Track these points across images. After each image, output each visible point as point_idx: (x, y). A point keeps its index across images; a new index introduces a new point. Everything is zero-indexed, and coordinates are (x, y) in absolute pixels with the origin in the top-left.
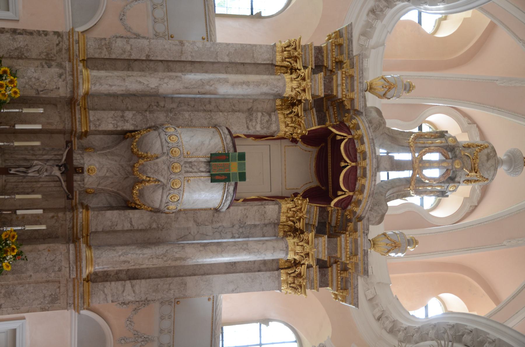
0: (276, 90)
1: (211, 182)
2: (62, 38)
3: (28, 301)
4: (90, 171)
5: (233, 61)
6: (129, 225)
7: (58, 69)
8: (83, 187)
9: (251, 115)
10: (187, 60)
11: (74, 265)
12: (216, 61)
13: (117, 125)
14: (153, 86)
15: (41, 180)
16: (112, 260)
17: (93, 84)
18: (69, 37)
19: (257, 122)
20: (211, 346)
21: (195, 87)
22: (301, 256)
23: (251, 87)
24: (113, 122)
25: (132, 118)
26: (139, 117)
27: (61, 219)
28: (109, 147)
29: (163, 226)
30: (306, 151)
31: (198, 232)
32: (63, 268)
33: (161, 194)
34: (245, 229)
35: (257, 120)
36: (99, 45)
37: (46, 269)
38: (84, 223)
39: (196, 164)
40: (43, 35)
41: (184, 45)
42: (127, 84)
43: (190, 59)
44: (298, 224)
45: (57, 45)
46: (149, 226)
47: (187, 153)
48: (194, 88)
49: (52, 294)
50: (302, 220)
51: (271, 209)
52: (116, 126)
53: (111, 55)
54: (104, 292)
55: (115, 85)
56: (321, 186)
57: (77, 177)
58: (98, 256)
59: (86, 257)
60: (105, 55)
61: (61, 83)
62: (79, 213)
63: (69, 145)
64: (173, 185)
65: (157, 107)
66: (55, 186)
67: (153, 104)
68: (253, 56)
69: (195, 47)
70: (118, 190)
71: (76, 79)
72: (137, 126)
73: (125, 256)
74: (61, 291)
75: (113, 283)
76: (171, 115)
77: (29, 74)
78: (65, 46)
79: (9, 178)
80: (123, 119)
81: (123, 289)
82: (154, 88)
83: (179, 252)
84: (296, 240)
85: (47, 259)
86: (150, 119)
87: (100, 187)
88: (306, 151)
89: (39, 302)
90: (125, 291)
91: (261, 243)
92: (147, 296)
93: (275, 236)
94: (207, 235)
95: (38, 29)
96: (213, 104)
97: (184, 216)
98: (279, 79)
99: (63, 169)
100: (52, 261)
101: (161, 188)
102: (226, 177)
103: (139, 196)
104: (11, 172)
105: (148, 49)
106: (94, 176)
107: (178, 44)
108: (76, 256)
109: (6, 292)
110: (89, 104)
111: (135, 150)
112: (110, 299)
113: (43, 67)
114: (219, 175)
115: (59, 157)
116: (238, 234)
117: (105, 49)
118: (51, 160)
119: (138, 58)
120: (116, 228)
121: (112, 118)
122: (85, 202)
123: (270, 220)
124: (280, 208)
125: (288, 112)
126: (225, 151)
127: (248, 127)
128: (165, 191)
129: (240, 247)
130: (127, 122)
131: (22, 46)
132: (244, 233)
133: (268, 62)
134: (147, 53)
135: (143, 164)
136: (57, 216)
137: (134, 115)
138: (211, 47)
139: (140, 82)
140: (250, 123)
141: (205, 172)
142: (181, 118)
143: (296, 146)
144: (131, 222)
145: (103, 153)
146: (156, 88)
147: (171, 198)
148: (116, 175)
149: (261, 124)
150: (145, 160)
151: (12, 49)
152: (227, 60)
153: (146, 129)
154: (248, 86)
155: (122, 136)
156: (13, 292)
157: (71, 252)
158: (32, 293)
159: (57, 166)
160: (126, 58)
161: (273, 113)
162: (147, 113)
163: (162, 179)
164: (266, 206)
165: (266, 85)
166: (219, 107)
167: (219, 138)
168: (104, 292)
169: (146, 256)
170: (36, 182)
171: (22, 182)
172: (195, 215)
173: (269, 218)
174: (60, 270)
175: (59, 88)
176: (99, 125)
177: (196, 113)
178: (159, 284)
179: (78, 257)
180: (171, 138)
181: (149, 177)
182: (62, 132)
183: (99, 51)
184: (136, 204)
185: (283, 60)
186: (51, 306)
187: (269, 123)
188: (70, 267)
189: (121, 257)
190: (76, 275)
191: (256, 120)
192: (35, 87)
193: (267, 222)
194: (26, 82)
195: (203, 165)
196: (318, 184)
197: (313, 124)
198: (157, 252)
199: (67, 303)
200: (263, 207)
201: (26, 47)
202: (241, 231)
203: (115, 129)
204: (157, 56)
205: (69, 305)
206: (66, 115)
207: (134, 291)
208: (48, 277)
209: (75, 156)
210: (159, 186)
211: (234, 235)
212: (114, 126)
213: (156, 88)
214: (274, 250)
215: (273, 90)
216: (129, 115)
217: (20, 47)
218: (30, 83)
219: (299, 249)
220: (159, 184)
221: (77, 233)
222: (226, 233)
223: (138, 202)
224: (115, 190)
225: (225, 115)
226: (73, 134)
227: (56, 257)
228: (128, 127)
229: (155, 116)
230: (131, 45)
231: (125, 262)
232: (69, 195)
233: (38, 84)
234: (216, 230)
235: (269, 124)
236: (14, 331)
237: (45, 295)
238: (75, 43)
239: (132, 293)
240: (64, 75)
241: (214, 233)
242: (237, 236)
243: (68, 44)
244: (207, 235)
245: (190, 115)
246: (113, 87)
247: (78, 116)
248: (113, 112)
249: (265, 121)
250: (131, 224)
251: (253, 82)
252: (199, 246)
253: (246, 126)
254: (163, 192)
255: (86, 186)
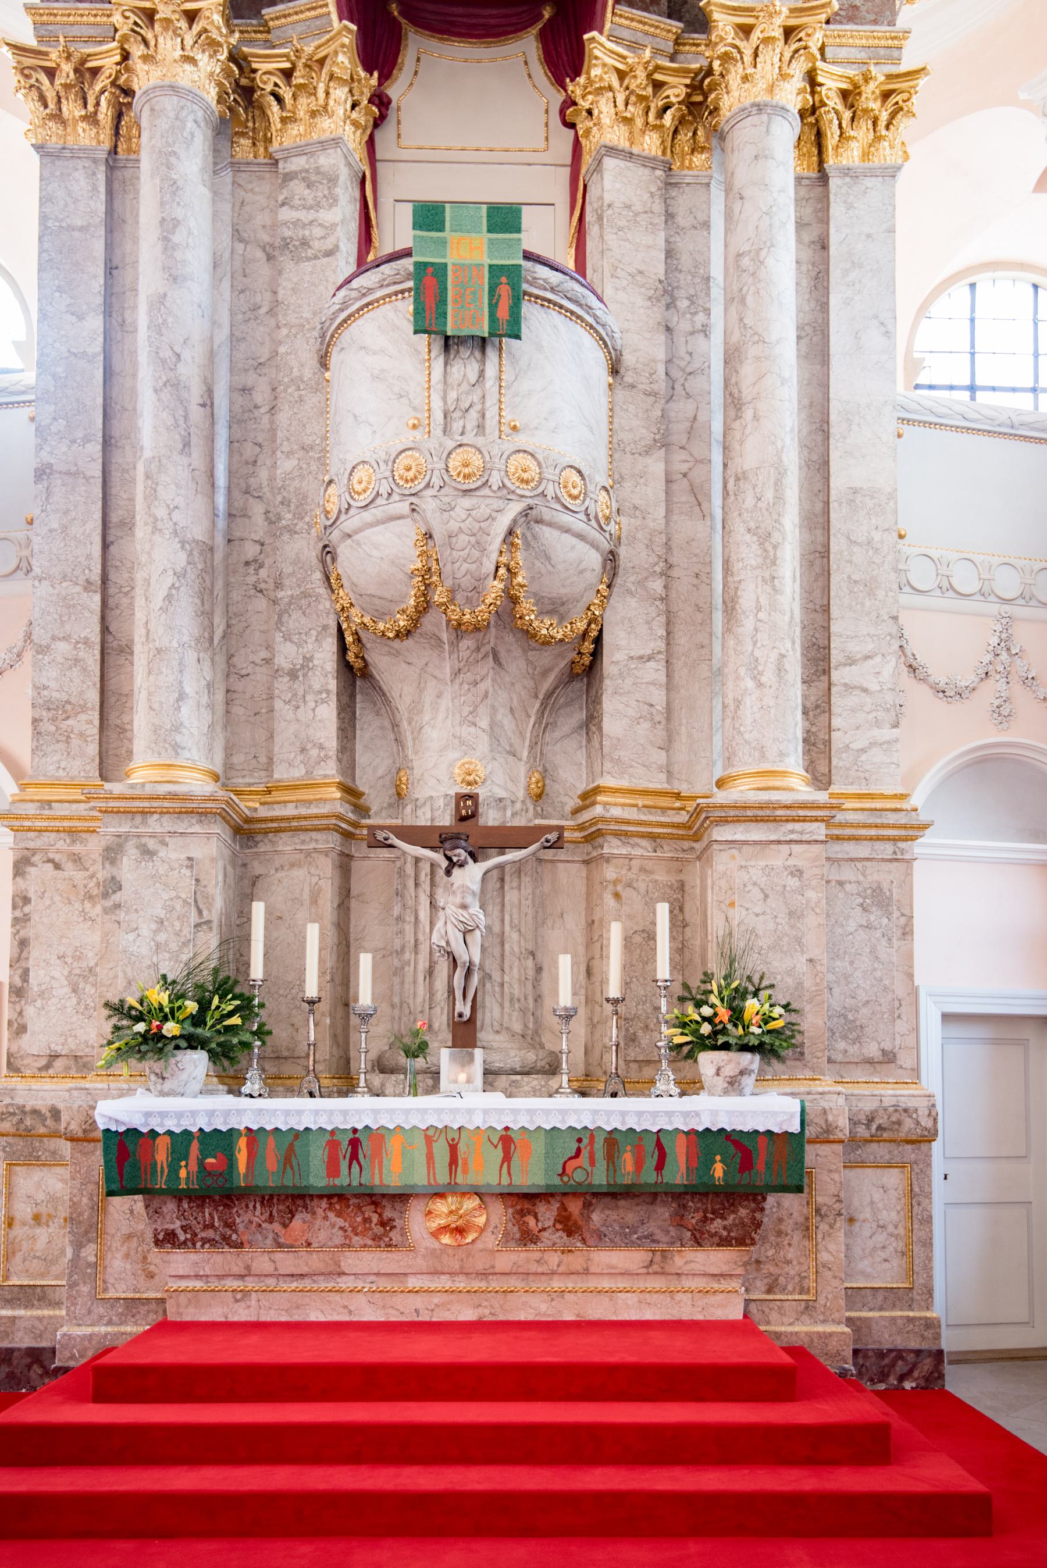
0: (190, 125)
1: (518, 337)
2: (34, 851)
3: (878, 974)
4: (471, 778)
5: (100, 300)
6: (652, 664)
7: (125, 859)
8: (523, 802)
9: (286, 244)
10: (99, 455)
11: (783, 829)
12: (102, 358)
13: (320, 692)
14: (183, 557)
15: (496, 929)
16: (773, 711)
17: (177, 754)
18: (30, 830)
19: (311, 223)
20: (1040, 441)
21: (181, 412)
22: (792, 57)
23: (179, 213)
24: (312, 704)
25: (299, 645)
26: (295, 621)
27: (624, 872)
28: (395, 725)
29: (659, 557)
30: (416, 73)
31: (682, 448)
32: (791, 862)
33: (556, 533)
34: (678, 287)
35: (306, 221)
36: (58, 742)
37: (791, 914)
38: (640, 803)
39: (452, 395)
40: (27, 909)
41: (50, 466)
42: (176, 645)
43: (95, 448)
44: (669, 92)
45: (57, 866)
46: (658, 603)
47: (414, 427)
48: (186, 418)
49: (861, 905)
50: (658, 76)
51: (618, 185)
52: (324, 695)
53: (89, 705)
54: (863, 751)
55: (181, 682)
56: (540, 25)
57: (490, 817)
58: (757, 754)
59: (758, 789)
60: (90, 722)
61: (174, 853)
62: (608, 815)
63: (380, 835)
64: (527, 482)
65: (261, 566)
66: (519, 888)
67: (252, 579)
68: (81, 229)
69: (54, 429)
70: (536, 696)
71: (155, 804)
72: (325, 627)
73: (760, 668)
74: (853, 878)
75: (836, 722)
76: (289, 516)
77: (144, 951)
78: (62, 843)
79: (487, 1021)
80: (300, 674)
81: (856, 692)
82: (190, 554)
83: (758, 490)
84: (734, 78)
85: (758, 910)
86: (299, 586)
87: (525, 754)
88: (416, 73)
89: (884, 942)
90: (865, 685)
91: (737, 206)
92: (886, 617)
93: (708, 185)
94: (695, 418)
95: (9, 922)
96: (250, 379)
97: (628, 484)
98: (152, 110)
99: (461, 854)
100: (766, 896)
101: (537, 528)
102: (504, 280)
103: (562, 619)
104: (467, 1013)
105: (65, 584)
106: (490, 767)
107: (45, 483)
108: (756, 820)
109: (844, 1037)
110: (252, 781)
111: (402, 623)
112: (886, 733)
113: (118, 906)
114: (493, 307)
115: (425, 868)
116: (696, 313)
117: (70, 722)
118: (432, 896)
119: (96, 619)
120: (660, 705)
121: (298, 707)
122: (573, 802)
123: (652, 195)
124: (612, 151)
125: (275, 107)
126: (409, 290)
127: (329, 254)
128: (547, 515)
129: (750, 280)
130: (310, 659)
131: (66, 973)
132: (692, 292)
133: (101, 177)
134: (78, 589)
135: (452, 591)
136: (615, 883)
137: (287, 638)
138: (54, 376)
139: (169, 598)
140: (316, 244)
141: (483, 361)
142: (296, 483)
143: (399, 109)
144: (641, 658)
145: (414, 739)
146: (187, 546)
147: (575, 498)
148: (486, 696)
149: (317, 206)
150: (435, 578)
151: (74, 1000)
152: (95, 323)
153: (333, 591)
154: (176, 223)
155: (358, 683)
156: (845, 1017)
157: (739, 837)
158: (852, 963)
159: (448, 872)
160: (98, 657)
161: (281, 165)
162: (280, 594)
163: (504, 522)
164: (606, 202)
165: (173, 160)
166: (261, 360)
167: (360, 322)
168: (863, 751)
169: (764, 601)
170: (502, 944)
171: (502, 985)
172: (628, 449)
173: (647, 196)
174: (797, 873)
175: (190, 859)
176: (321, 747)
177: (279, 434)
178: (849, 577)
179: (760, 813)
180: (358, 488)
181: (497, 568)
182: (345, 865)
183: (75, 742)
184: (584, 635)
185: (92, 119)
186: (899, 909)
187: (313, 178)
188: (790, 842)
189: (764, 679)
190: (816, 825)
191: (304, 226)
192: (186, 931)
193: (658, 207)
194: (170, 959)
195: (457, 369)
196: (534, 30)
197: (321, 16)
198: (754, 563)
199: (890, 860)
200: (610, 212)
201: (69, 960)
202: (686, 303)
203: (334, 698)
204: (89, 557)
205: (899, 857)
206: (286, 844)
207: (867, 657)
208: (818, 910)
209: (423, 819)
210: (529, 535)
211: (699, 326)
212: (323, 701)
213: (187, 546)
214: (766, 157)
215: (192, 135)
216: (286, 654)
217: (67, 977)
218: (174, 946)
219: (768, 67)
220: (523, 535)
221: (673, 825)
222: (691, 354)
223: (581, 626)
224: (537, 705)
225: (287, 336)
226: (350, 829)
227: (755, 884)
228: (326, 655)
229: (290, 570)
230: (54, 638)
231: (780, 669)
232: (547, 841)
233: (177, 924)
234: (677, 386)
235: (319, 178)
236: (947, 1018)
237: (861, 926)
238: (47, 812)
239: (870, 662)
240: (144, 840)
241: (688, 396)
242: (700, 318)
243: (53, 835)
244: (695, 418)
245: (289, 454)
246: (188, 689)
247: (290, 811)
248: (278, 704)
249: (307, 192)
250: (650, 659)
251: (162, 204)
252: (736, 425)
253: (325, 260)
254: (550, 524)
255: (521, 794)
